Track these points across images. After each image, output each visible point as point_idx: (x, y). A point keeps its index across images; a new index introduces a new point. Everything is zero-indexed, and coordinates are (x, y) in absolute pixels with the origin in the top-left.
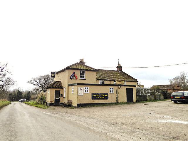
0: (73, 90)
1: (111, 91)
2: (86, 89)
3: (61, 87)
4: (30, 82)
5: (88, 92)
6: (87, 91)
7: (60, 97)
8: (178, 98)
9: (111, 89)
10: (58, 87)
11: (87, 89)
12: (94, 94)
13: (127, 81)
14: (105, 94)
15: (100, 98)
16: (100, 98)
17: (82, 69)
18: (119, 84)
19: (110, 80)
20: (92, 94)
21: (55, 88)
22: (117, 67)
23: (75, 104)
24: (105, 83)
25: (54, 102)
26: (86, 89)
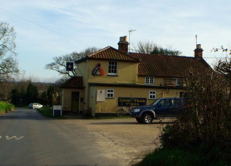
1: (151, 96)
2: (109, 93)
4: (51, 66)
5: (113, 97)
6: (112, 95)
9: (151, 93)
11: (111, 93)
12: (123, 98)
14: (140, 99)
20: (119, 99)
21: (72, 88)
26: (110, 93)
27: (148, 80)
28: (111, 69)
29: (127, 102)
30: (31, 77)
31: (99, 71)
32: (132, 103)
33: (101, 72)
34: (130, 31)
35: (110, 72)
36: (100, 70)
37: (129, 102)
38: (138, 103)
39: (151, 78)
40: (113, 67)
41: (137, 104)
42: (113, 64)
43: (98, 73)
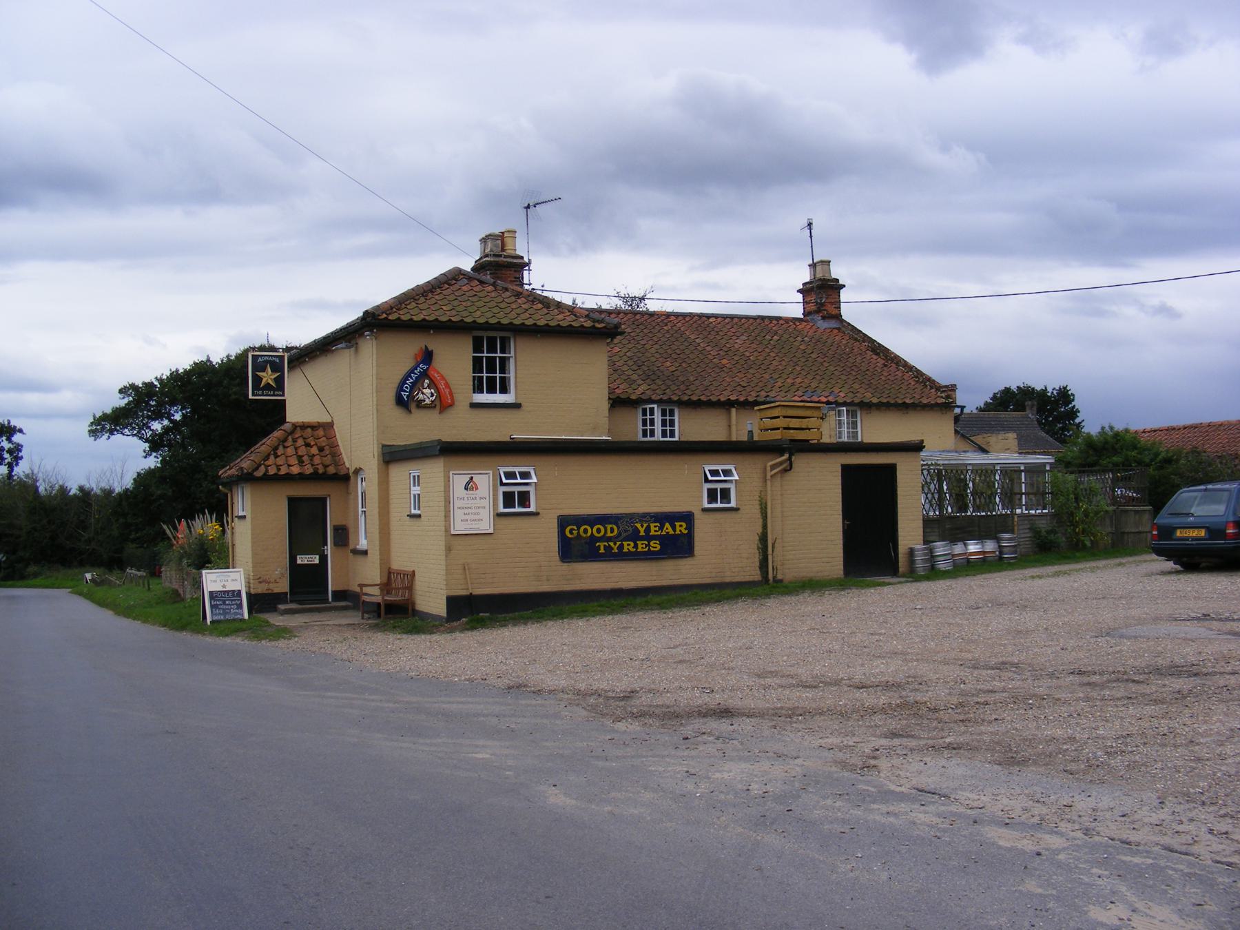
0: (416, 490)
3: (331, 470)
5: (532, 509)
6: (524, 499)
7: (329, 549)
8: (1194, 533)
10: (309, 470)
12: (580, 520)
13: (866, 406)
14: (662, 518)
15: (628, 546)
16: (628, 546)
17: (487, 326)
18: (776, 435)
19: (728, 405)
20: (564, 522)
21: (288, 478)
22: (805, 291)
23: (432, 600)
24: (688, 427)
25: (283, 586)
27: (652, 422)
28: (498, 375)
29: (600, 539)
30: (35, 472)
31: (429, 387)
32: (626, 539)
33: (438, 390)
34: (528, 207)
35: (478, 389)
36: (431, 380)
37: (609, 539)
38: (655, 538)
39: (664, 413)
40: (491, 361)
41: (649, 545)
42: (492, 349)
43: (427, 395)
